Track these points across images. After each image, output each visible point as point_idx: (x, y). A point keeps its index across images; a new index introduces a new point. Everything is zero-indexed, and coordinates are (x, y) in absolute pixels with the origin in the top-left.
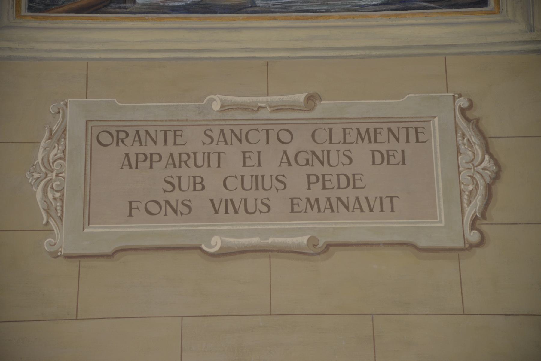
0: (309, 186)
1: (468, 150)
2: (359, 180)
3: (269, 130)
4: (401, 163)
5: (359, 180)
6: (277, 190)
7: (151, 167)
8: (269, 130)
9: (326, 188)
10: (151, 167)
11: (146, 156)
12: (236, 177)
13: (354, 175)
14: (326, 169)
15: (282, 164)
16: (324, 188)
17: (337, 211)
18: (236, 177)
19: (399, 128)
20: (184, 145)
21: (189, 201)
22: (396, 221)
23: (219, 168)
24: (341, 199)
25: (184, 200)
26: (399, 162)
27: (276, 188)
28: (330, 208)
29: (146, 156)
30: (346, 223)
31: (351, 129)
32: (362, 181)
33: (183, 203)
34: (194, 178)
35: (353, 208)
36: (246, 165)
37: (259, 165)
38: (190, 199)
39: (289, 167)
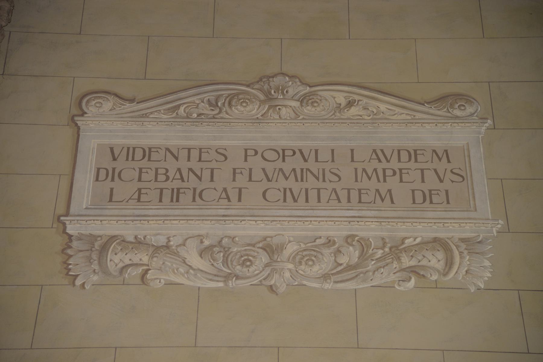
1: (207, 258)
2: (366, 194)
3: (214, 169)
5: (366, 194)
8: (214, 169)
12: (134, 169)
13: (430, 191)
14: (321, 185)
15: (220, 200)
16: (401, 181)
18: (134, 169)
19: (202, 169)
23: (235, 182)
24: (192, 169)
25: (331, 169)
27: (450, 180)
30: (91, 163)
31: (150, 168)
33: (452, 171)
36: (317, 190)
37: (333, 161)
39: (296, 183)
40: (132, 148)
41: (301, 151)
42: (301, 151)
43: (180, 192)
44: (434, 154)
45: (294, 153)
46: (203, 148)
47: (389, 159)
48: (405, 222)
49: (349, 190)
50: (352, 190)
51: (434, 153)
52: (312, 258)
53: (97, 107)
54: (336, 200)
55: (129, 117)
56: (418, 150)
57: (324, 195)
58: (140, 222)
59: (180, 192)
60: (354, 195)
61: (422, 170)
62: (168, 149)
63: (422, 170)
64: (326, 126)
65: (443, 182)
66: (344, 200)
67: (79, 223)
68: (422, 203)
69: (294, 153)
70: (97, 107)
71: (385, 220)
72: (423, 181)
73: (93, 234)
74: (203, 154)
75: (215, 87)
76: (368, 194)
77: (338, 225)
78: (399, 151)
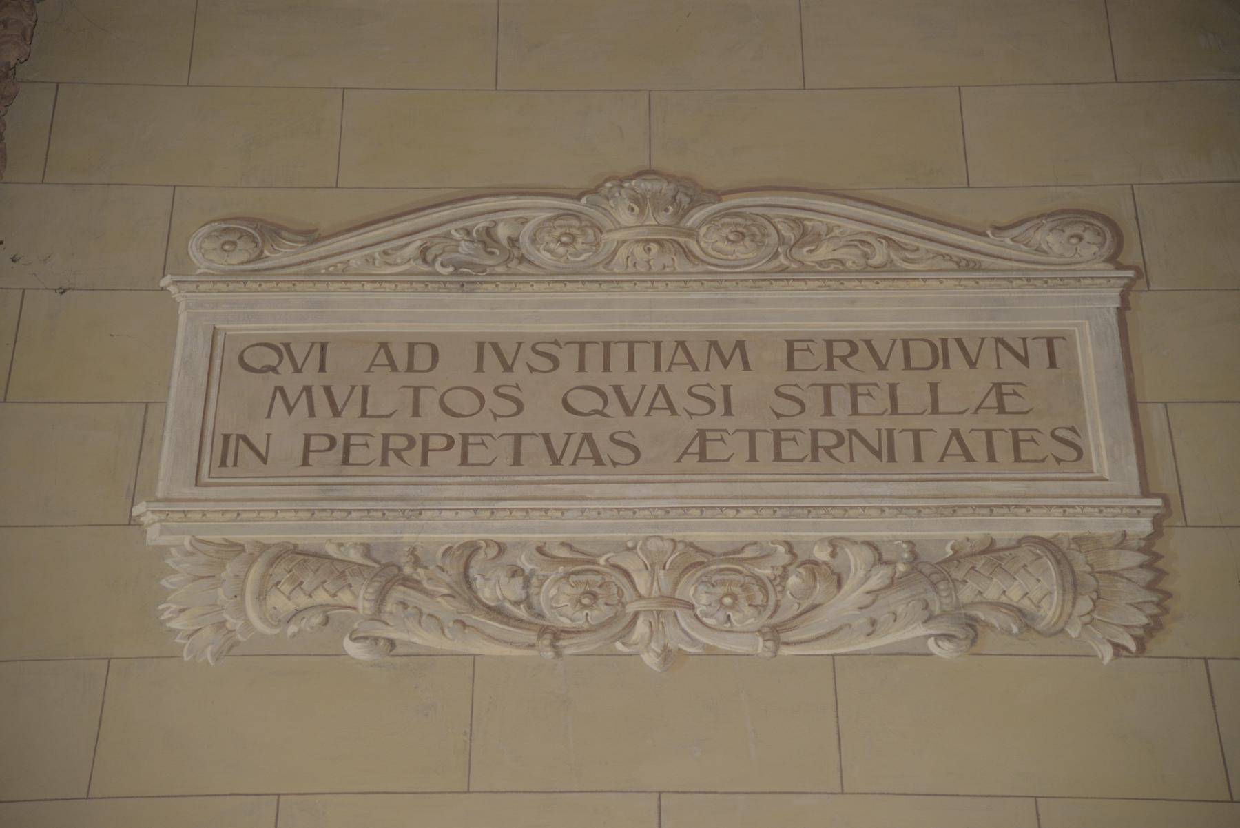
0: (942, 457)
2: (719, 440)
4: (809, 458)
5: (719, 440)
6: (496, 416)
7: (424, 462)
9: (412, 389)
10: (424, 462)
11: (333, 441)
17: (1027, 341)
20: (972, 430)
21: (517, 387)
22: (695, 324)
26: (805, 457)
28: (592, 459)
29: (333, 441)
32: (726, 441)
34: (829, 344)
35: (683, 450)
38: (517, 384)
40: (901, 342)
41: (868, 343)
42: (868, 343)
43: (430, 448)
44: (713, 351)
45: (854, 350)
46: (417, 344)
47: (884, 361)
48: (298, 510)
49: (752, 434)
50: (709, 433)
51: (712, 349)
52: (734, 588)
53: (225, 251)
54: (589, 458)
55: (296, 274)
56: (637, 342)
57: (931, 448)
58: (368, 513)
59: (430, 448)
60: (1003, 445)
61: (417, 390)
62: (1000, 341)
63: (417, 390)
64: (1093, 285)
65: (632, 415)
66: (980, 453)
67: (906, 514)
68: (633, 462)
69: (854, 350)
70: (225, 251)
71: (609, 505)
72: (416, 413)
73: (1045, 537)
74: (796, 354)
75: (550, 202)
76: (485, 445)
77: (784, 517)
78: (906, 343)
